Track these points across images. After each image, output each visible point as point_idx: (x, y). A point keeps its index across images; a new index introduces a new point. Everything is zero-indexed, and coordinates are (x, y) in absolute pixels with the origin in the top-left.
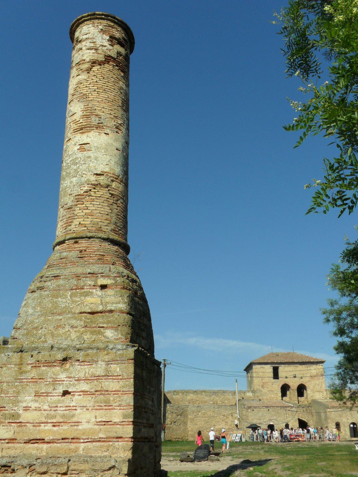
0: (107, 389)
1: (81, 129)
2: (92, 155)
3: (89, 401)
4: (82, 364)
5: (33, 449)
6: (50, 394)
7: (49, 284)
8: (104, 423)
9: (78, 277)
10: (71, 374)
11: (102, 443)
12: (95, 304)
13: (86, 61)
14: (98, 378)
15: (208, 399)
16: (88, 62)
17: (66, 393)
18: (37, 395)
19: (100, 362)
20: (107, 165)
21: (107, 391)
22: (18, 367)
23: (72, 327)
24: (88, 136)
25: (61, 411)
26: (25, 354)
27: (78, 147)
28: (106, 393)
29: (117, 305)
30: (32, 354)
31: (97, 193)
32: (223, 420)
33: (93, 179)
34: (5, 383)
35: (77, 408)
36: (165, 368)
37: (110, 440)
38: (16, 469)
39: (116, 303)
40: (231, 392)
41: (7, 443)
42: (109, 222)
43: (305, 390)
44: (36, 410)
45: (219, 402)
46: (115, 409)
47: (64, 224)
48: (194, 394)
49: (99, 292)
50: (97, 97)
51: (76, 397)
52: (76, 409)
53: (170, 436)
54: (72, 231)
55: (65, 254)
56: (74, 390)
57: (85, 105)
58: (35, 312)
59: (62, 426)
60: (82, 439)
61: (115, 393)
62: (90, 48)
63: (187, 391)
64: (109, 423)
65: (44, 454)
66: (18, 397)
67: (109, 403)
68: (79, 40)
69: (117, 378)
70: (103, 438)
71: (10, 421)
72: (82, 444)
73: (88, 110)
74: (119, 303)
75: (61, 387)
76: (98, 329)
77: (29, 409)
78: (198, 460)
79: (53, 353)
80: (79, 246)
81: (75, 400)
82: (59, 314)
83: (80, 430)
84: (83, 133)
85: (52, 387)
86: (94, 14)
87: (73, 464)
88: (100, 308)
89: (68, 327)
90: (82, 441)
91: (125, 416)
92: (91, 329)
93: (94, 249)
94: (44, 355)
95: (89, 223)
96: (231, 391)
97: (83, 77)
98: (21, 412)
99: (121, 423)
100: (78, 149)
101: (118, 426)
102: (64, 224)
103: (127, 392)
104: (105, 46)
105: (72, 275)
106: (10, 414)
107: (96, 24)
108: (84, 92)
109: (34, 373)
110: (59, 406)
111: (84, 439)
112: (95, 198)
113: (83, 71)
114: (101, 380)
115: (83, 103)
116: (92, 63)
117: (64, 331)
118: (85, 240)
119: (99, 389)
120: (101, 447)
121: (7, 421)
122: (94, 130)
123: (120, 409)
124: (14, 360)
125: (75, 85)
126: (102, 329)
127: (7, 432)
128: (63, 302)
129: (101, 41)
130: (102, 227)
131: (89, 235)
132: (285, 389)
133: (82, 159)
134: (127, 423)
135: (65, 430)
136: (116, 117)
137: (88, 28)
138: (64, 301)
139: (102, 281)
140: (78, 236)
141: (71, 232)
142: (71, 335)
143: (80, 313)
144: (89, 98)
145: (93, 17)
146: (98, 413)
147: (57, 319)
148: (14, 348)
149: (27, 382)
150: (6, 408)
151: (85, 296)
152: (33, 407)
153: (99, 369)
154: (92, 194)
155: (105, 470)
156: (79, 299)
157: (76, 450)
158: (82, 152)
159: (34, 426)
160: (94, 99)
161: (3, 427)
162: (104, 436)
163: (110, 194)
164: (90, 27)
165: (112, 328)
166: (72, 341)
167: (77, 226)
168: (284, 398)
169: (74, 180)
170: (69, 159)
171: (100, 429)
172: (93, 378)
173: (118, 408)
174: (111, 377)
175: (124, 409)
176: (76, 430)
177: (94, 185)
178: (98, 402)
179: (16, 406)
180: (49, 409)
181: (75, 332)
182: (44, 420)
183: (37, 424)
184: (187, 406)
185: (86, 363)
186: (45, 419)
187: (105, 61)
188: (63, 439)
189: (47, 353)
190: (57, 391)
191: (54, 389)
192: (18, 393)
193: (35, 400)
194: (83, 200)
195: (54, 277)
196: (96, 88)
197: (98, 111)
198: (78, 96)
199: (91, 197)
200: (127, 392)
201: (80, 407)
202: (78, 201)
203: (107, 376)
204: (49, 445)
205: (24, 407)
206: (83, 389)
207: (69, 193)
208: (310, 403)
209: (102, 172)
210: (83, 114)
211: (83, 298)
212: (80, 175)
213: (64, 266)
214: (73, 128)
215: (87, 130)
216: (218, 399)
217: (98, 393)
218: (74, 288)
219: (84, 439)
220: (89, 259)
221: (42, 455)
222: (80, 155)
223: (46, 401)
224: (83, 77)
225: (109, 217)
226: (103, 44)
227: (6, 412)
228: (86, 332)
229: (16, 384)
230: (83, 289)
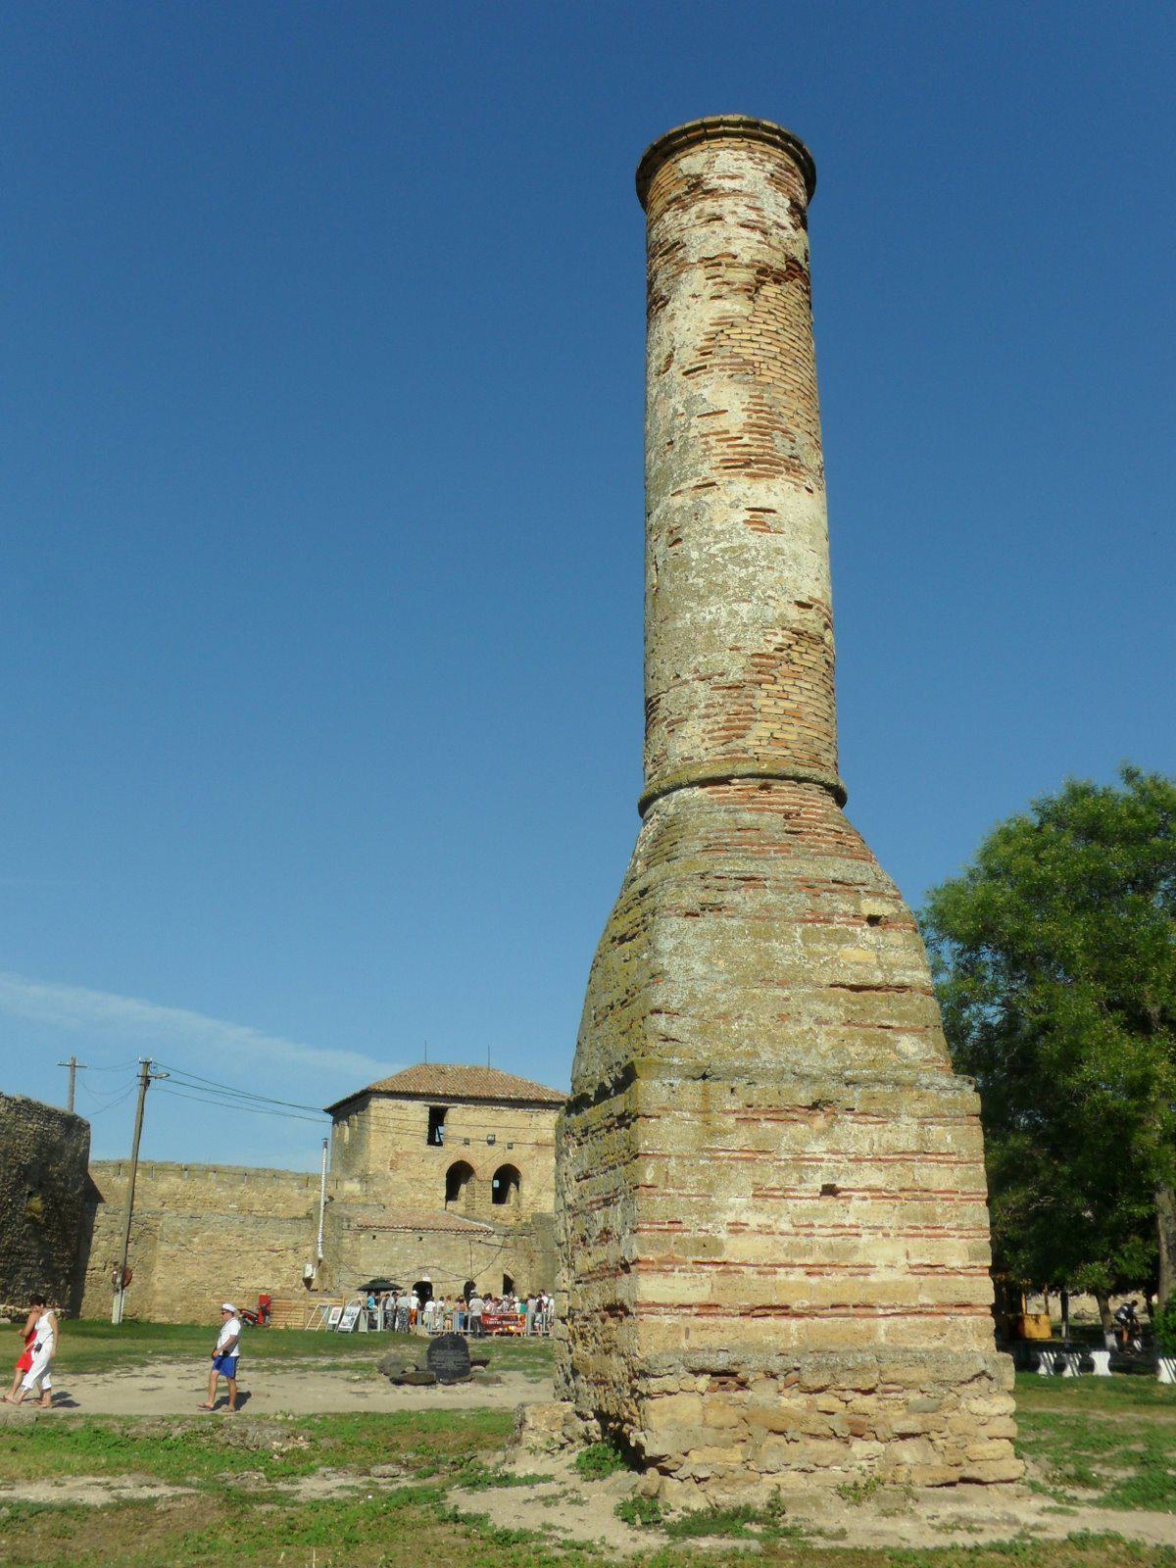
0: (925, 1187)
2: (785, 547)
3: (886, 1214)
6: (791, 1194)
9: (809, 886)
10: (837, 1144)
11: (928, 1319)
12: (866, 965)
13: (739, 260)
14: (904, 1156)
15: (224, 1193)
16: (747, 266)
17: (829, 1190)
18: (761, 1193)
21: (926, 1191)
22: (700, 1117)
23: (819, 1021)
24: (769, 490)
25: (822, 1238)
27: (747, 515)
28: (926, 1195)
29: (915, 973)
30: (734, 1085)
32: (266, 1264)
34: (673, 1158)
36: (145, 1089)
37: (946, 1310)
38: (751, 1379)
40: (296, 1176)
41: (697, 1315)
43: (513, 1185)
44: (760, 1232)
45: (257, 1207)
46: (949, 1236)
47: (720, 729)
48: (180, 1176)
49: (869, 934)
50: (784, 378)
51: (856, 1203)
52: (857, 1235)
53: (98, 1305)
54: (751, 753)
56: (850, 1185)
57: (753, 394)
58: (712, 971)
59: (828, 1275)
60: (880, 1307)
61: (945, 1196)
62: (747, 223)
63: (161, 1164)
64: (939, 1270)
65: (795, 1343)
66: (710, 1196)
67: (934, 1220)
69: (947, 1158)
70: (928, 1306)
71: (700, 1258)
72: (881, 1319)
73: (762, 411)
76: (880, 1031)
77: (743, 1230)
78: (447, 1381)
81: (857, 1210)
82: (782, 984)
83: (873, 1285)
86: (756, 125)
87: (893, 1366)
88: (878, 978)
89: (808, 1019)
90: (881, 1312)
91: (974, 1254)
92: (862, 1031)
93: (817, 814)
94: (764, 1092)
95: (795, 737)
96: (298, 1175)
97: (737, 308)
98: (723, 1236)
99: (965, 1272)
100: (746, 522)
101: (961, 1278)
102: (720, 729)
103: (973, 1196)
104: (783, 228)
105: (795, 880)
106: (696, 1241)
108: (746, 353)
109: (741, 1139)
110: (816, 1225)
111: (885, 1308)
113: (736, 290)
114: (909, 1163)
115: (746, 387)
118: (790, 785)
119: (908, 1184)
120: (928, 1327)
121: (690, 1259)
122: (781, 473)
123: (961, 1237)
124: (687, 1098)
125: (711, 325)
126: (889, 1033)
127: (693, 1286)
130: (821, 753)
132: (459, 1174)
133: (763, 553)
134: (980, 1271)
138: (788, 950)
139: (871, 906)
140: (775, 772)
141: (745, 756)
142: (820, 1042)
143: (832, 986)
144: (761, 375)
145: (751, 132)
147: (778, 998)
148: (687, 1065)
149: (729, 1158)
150: (685, 1226)
151: (840, 942)
152: (753, 1226)
153: (904, 1133)
154: (795, 656)
155: (963, 1383)
157: (870, 1334)
158: (760, 533)
159: (760, 1273)
161: (682, 1274)
162: (930, 1302)
164: (743, 160)
165: (912, 1031)
166: (824, 1057)
167: (764, 743)
168: (450, 1203)
169: (744, 608)
171: (921, 1284)
172: (891, 1157)
174: (934, 1157)
175: (969, 1237)
176: (863, 1285)
177: (797, 634)
178: (908, 1218)
179: (708, 1221)
180: (793, 1230)
181: (828, 1034)
182: (782, 1258)
183: (766, 1269)
184: (156, 1213)
185: (871, 1119)
186: (787, 1255)
188: (833, 1307)
189: (772, 1087)
190: (808, 1186)
191: (801, 1180)
193: (755, 1207)
194: (773, 671)
196: (778, 350)
197: (785, 420)
200: (973, 1196)
201: (869, 1228)
204: (802, 1322)
205: (729, 1224)
207: (729, 645)
208: (526, 1224)
209: (811, 599)
210: (751, 421)
211: (835, 947)
213: (758, 852)
214: (721, 454)
216: (254, 1196)
217: (906, 1194)
218: (809, 917)
219: (885, 1308)
221: (789, 1346)
222: (752, 539)
223: (784, 1212)
224: (737, 308)
229: (702, 1162)
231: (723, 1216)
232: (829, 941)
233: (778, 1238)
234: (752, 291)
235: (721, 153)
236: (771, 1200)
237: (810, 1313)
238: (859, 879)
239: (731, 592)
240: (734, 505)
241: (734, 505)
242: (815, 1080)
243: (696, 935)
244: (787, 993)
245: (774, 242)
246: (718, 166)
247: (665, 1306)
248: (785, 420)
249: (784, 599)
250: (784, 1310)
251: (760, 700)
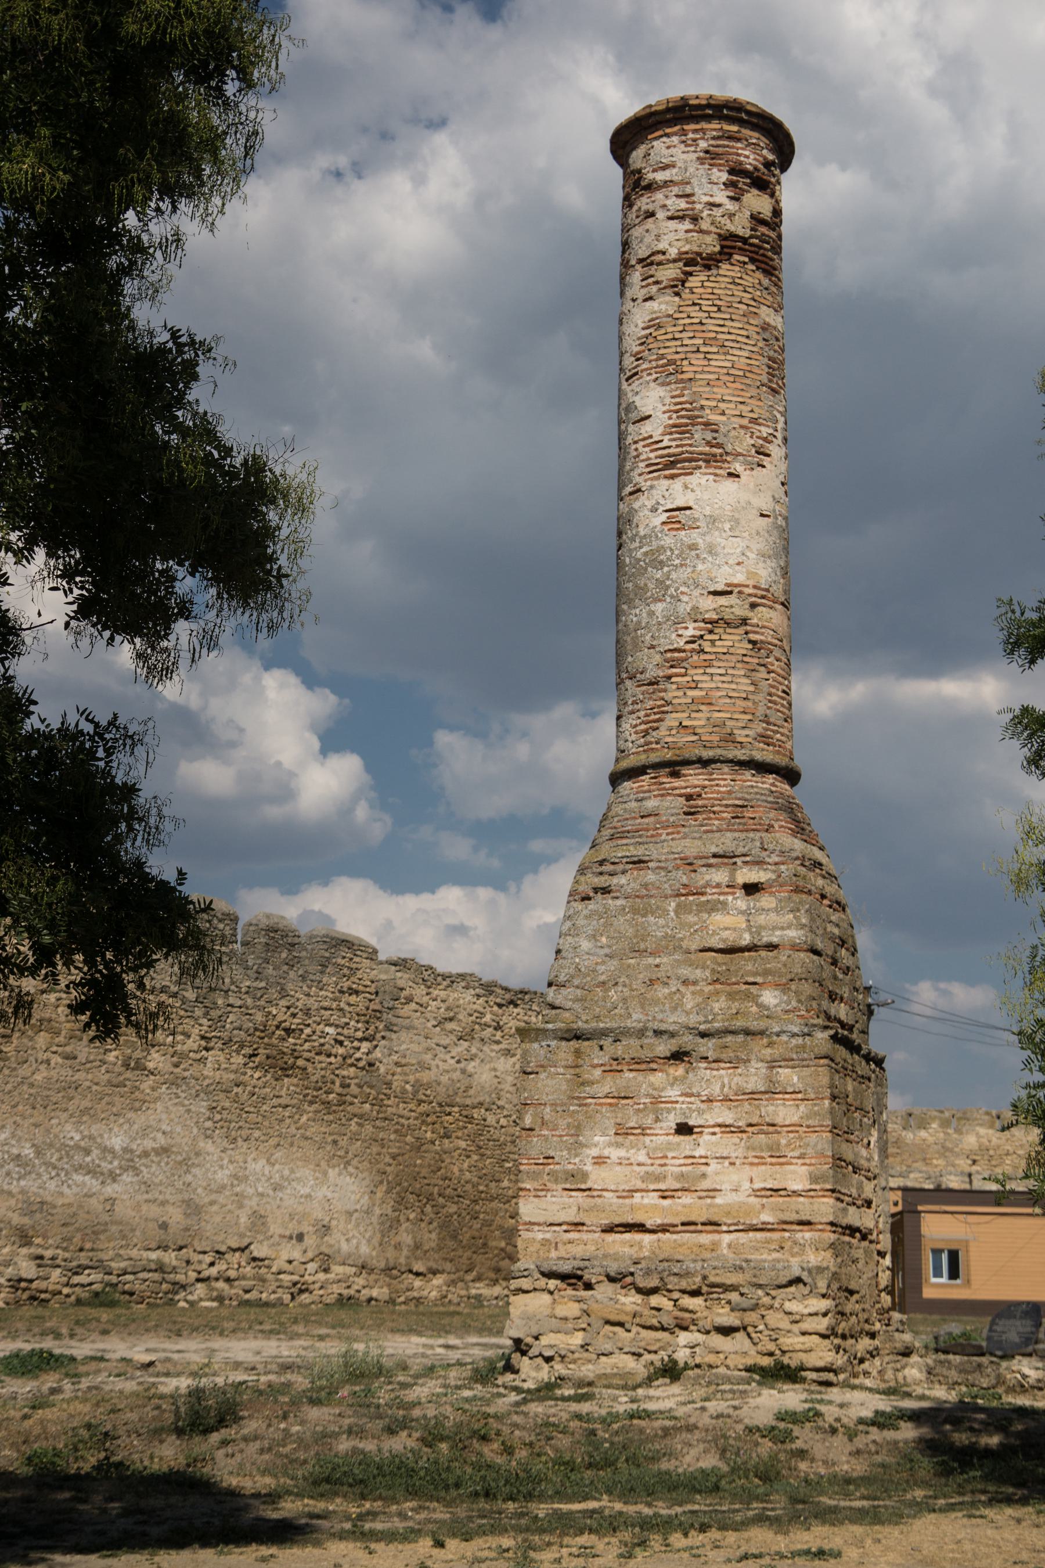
1: (672, 465)
3: (731, 1145)
4: (714, 1065)
5: (622, 1244)
7: (623, 880)
8: (769, 1193)
11: (768, 1235)
13: (668, 256)
14: (753, 1095)
16: (675, 261)
18: (623, 1132)
19: (753, 1063)
20: (739, 564)
22: (572, 1071)
23: (685, 982)
24: (686, 487)
26: (586, 1043)
27: (664, 517)
28: (771, 1129)
31: (718, 643)
33: (709, 605)
35: (708, 1161)
37: (785, 1227)
39: (782, 928)
42: (749, 717)
46: (791, 1164)
49: (740, 902)
50: (706, 369)
51: (706, 1137)
54: (662, 744)
55: (651, 804)
56: (701, 1122)
64: (782, 1193)
67: (778, 1150)
68: (643, 184)
69: (794, 1096)
71: (568, 1186)
74: (789, 927)
75: (672, 1116)
79: (646, 1041)
80: (683, 784)
81: (706, 1144)
84: (672, 477)
85: (652, 1116)
87: (713, 1272)
88: (746, 939)
90: (725, 1228)
91: (814, 1179)
92: (728, 988)
93: (719, 792)
95: (702, 723)
98: (589, 1167)
100: (664, 523)
101: (801, 1199)
106: (566, 1172)
107: (691, 135)
112: (713, 657)
116: (685, 265)
117: (667, 991)
119: (755, 1120)
122: (700, 467)
123: (804, 1164)
126: (753, 989)
128: (657, 926)
129: (705, 191)
131: (707, 754)
135: (687, 1205)
136: (754, 421)
137: (668, 147)
142: (686, 1004)
143: (701, 951)
146: (755, 1171)
148: (560, 1030)
150: (557, 1160)
153: (754, 1076)
156: (696, 919)
157: (714, 1247)
160: (698, 376)
162: (771, 1220)
163: (750, 641)
167: (674, 732)
170: (641, 547)
171: (763, 1205)
173: (800, 1161)
176: (710, 1205)
178: (754, 1149)
179: (576, 1156)
181: (693, 993)
182: (640, 1185)
185: (723, 1065)
187: (720, 253)
188: (683, 1224)
190: (664, 1125)
191: (657, 1120)
192: (578, 1127)
194: (684, 664)
195: (634, 863)
196: (701, 341)
197: (708, 411)
198: (654, 364)
199: (703, 657)
202: (672, 667)
203: (771, 1092)
204: (654, 1237)
206: (720, 1120)
207: (647, 644)
210: (671, 422)
211: (705, 916)
212: (672, 596)
213: (652, 836)
215: (683, 468)
218: (683, 891)
220: (710, 819)
225: (750, 704)
226: (711, 200)
227: (557, 1167)
228: (718, 993)
230: (702, 894)
231: (588, 1151)
232: (700, 911)
233: (637, 1169)
234: (677, 287)
235: (655, 143)
236: (631, 1137)
237: (664, 1229)
238: (741, 850)
239: (649, 594)
240: (654, 510)
241: (654, 510)
242: (672, 1035)
243: (586, 917)
244: (658, 961)
245: (705, 225)
246: (653, 158)
247: (539, 1224)
248: (708, 411)
249: (696, 593)
250: (639, 1227)
251: (672, 693)
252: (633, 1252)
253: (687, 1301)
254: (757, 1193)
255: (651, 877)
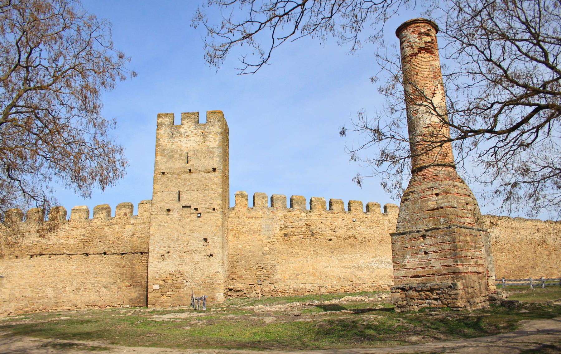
23: (424, 218)
81: (431, 256)
237: (423, 276)
252: (417, 282)
253: (427, 293)
254: (442, 266)
255: (415, 195)
